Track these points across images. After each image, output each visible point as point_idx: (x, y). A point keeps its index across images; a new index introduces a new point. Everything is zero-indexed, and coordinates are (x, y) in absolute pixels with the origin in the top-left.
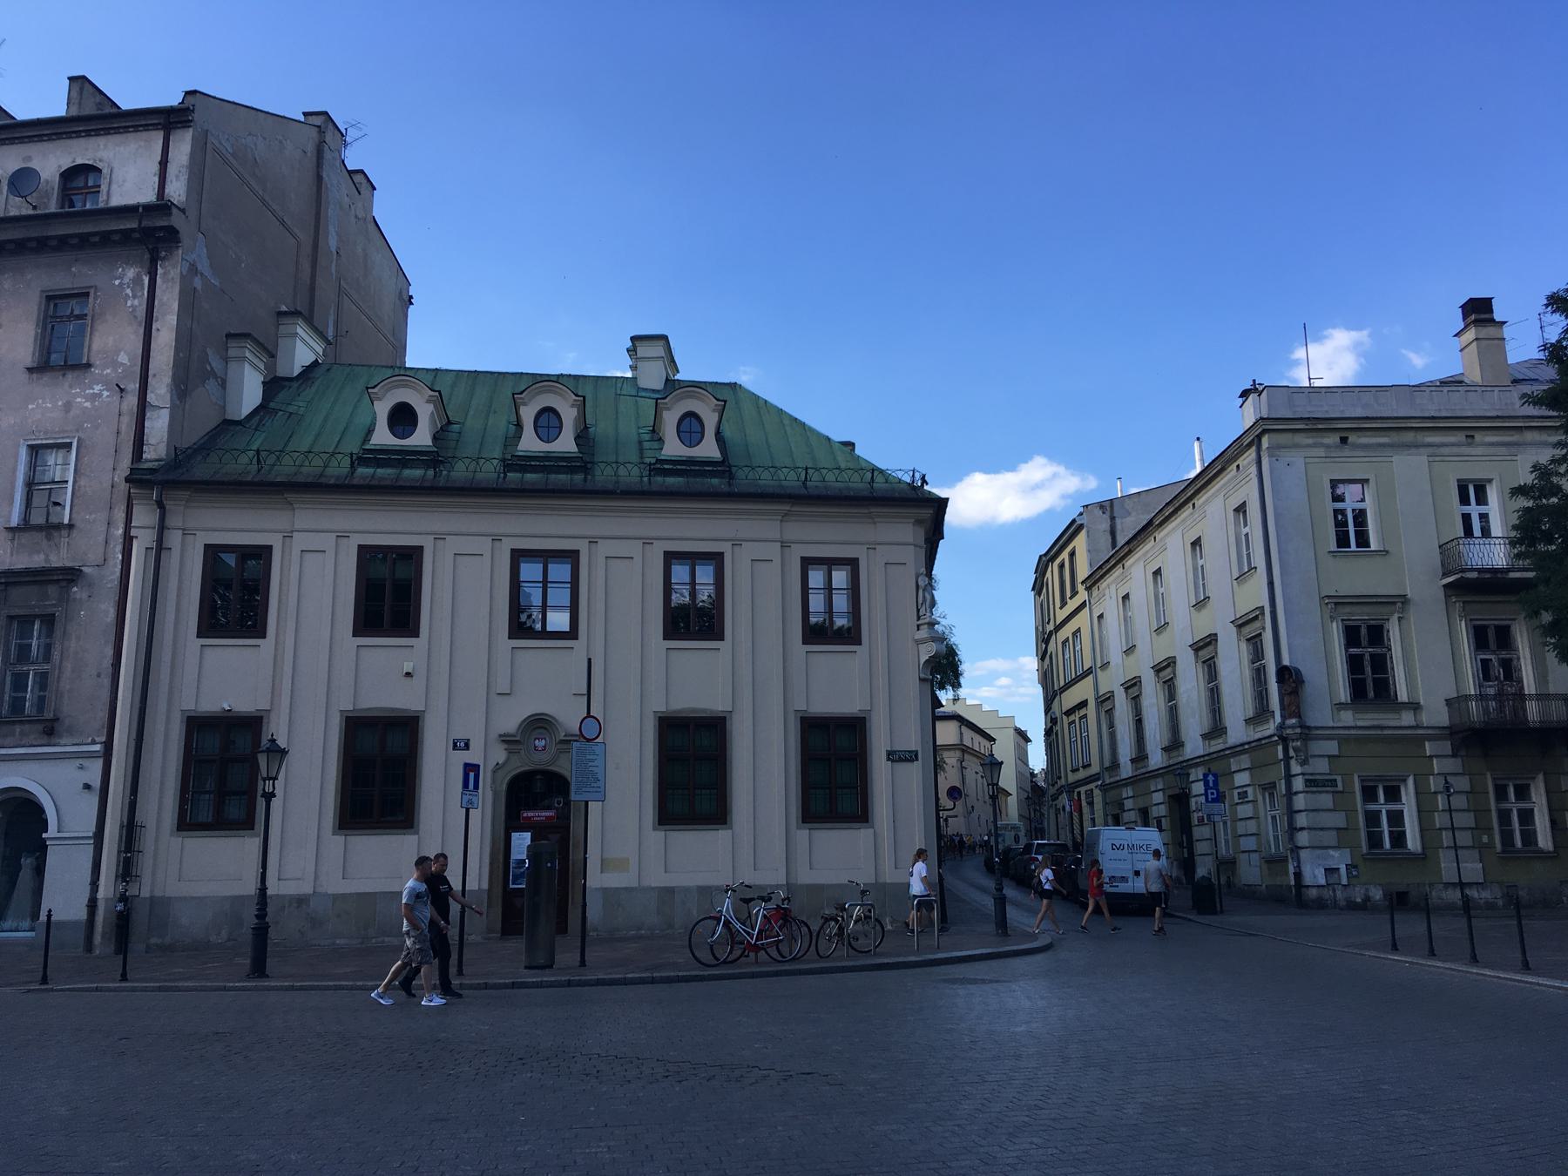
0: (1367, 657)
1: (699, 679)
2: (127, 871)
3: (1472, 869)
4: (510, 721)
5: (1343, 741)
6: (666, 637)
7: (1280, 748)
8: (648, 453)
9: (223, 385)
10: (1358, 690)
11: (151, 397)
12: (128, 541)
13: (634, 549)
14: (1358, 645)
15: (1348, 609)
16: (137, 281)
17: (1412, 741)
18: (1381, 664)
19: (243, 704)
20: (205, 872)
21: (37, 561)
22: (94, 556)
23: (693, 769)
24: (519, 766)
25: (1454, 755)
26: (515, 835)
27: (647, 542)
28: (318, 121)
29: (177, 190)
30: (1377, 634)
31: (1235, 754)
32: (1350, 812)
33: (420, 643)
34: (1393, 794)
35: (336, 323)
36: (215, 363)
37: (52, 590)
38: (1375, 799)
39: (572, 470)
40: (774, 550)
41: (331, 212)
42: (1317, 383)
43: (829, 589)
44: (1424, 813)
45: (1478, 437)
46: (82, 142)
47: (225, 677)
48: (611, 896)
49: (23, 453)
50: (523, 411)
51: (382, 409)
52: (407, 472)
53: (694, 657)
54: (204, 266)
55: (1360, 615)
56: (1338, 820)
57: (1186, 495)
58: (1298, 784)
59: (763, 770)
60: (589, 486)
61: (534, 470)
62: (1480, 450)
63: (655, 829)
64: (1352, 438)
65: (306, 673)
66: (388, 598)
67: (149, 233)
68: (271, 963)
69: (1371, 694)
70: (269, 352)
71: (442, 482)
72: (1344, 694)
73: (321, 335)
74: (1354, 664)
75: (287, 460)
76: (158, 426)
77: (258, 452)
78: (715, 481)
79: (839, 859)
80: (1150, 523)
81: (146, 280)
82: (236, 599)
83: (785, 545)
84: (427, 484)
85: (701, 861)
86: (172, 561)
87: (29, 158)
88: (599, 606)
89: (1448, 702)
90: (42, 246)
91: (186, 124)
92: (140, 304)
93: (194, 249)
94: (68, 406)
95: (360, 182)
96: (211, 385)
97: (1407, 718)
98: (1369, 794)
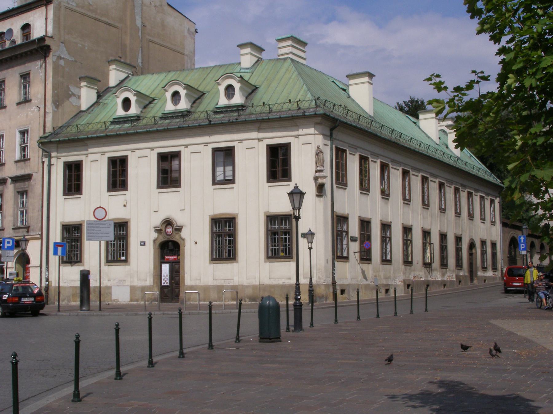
4: (157, 221)
11: (47, 110)
13: (200, 148)
16: (41, 66)
22: (36, 170)
23: (224, 236)
24: (162, 239)
26: (163, 265)
36: (73, 90)
48: (192, 287)
49: (18, 137)
59: (251, 238)
66: (168, 174)
67: (39, 49)
71: (242, 118)
81: (44, 65)
82: (74, 183)
87: (12, 24)
92: (42, 74)
94: (27, 115)
96: (73, 99)
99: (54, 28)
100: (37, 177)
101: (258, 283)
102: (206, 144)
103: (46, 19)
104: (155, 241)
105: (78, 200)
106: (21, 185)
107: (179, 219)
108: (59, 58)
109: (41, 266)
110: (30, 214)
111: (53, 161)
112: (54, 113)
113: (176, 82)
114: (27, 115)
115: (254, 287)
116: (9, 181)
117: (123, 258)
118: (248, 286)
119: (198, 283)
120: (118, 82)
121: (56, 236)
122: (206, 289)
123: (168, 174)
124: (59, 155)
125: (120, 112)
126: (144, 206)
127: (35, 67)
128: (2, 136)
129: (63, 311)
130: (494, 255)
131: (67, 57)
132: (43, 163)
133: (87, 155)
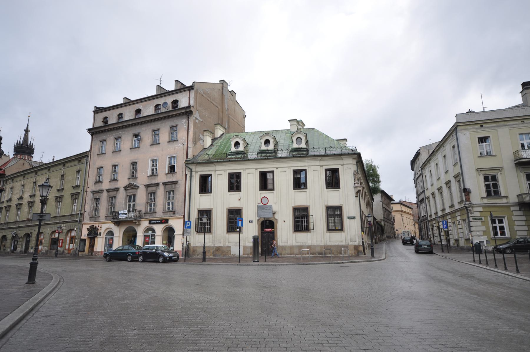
0: (491, 185)
1: (301, 198)
3: (484, 239)
5: (484, 207)
9: (203, 141)
10: (489, 194)
11: (189, 146)
12: (186, 175)
13: (222, 172)
14: (488, 181)
15: (484, 172)
16: (186, 122)
17: (507, 206)
18: (496, 186)
21: (170, 180)
22: (180, 178)
25: (520, 210)
27: (321, 166)
28: (222, 82)
29: (192, 103)
30: (494, 178)
31: (457, 212)
32: (487, 226)
34: (501, 221)
35: (228, 124)
36: (201, 136)
37: (173, 185)
38: (495, 223)
41: (226, 101)
42: (486, 110)
44: (511, 227)
45: (525, 121)
46: (158, 99)
47: (202, 202)
48: (283, 248)
49: (167, 159)
51: (233, 143)
53: (235, 195)
54: (198, 117)
55: (488, 173)
56: (484, 228)
57: (441, 145)
58: (471, 219)
61: (264, 153)
62: (526, 125)
64: (484, 125)
65: (220, 200)
66: (235, 183)
67: (187, 112)
69: (493, 194)
70: (213, 133)
72: (484, 194)
73: (224, 127)
74: (488, 186)
76: (190, 151)
79: (336, 239)
80: (434, 151)
82: (205, 185)
86: (193, 179)
89: (518, 196)
90: (169, 117)
91: (193, 89)
92: (186, 127)
93: (196, 115)
94: (175, 149)
95: (233, 93)
96: (201, 141)
97: (505, 201)
98: (493, 221)
99: (194, 102)
100: (181, 183)
101: (323, 244)
102: (289, 168)
103: (189, 98)
104: (258, 220)
105: (209, 197)
106: (169, 187)
108: (196, 118)
110: (176, 204)
111: (193, 174)
112: (193, 147)
113: (237, 137)
114: (175, 149)
115: (321, 247)
116: (161, 184)
117: (238, 230)
118: (317, 246)
119: (286, 244)
121: (194, 215)
122: (291, 247)
123: (235, 183)
127: (182, 123)
131: (199, 118)
132: (186, 175)
133: (215, 171)
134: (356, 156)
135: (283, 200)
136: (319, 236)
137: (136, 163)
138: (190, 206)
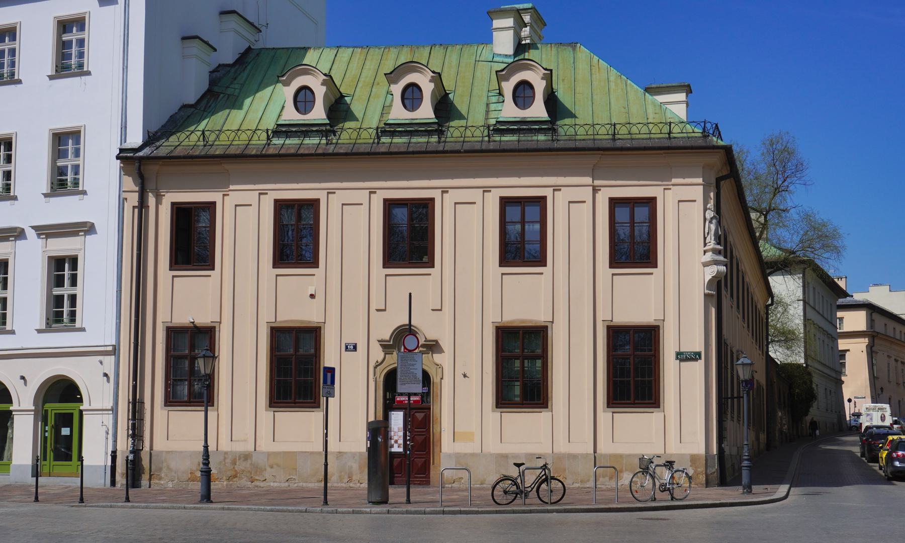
1: (525, 297)
2: (136, 433)
6: (275, 265)
7: (187, 363)
8: (493, 115)
19: (203, 320)
20: (176, 434)
33: (319, 272)
39: (429, 133)
40: (252, 197)
43: (632, 222)
48: (463, 463)
50: (504, 84)
52: (307, 141)
53: (407, 281)
59: (577, 367)
60: (556, 145)
61: (401, 134)
63: (493, 411)
66: (409, 239)
68: (39, 498)
71: (331, 149)
75: (223, 137)
77: (203, 132)
78: (541, 137)
82: (193, 244)
83: (595, 190)
84: (320, 151)
85: (526, 435)
88: (228, 242)
107: (428, 327)
109: (115, 410)
120: (237, 56)
123: (409, 239)
124: (597, 183)
125: (291, 115)
126: (351, 297)
128: (8, 144)
129: (46, 501)
130: (732, 412)
134: (716, 160)
135: (465, 296)
136: (576, 423)
137: (75, 135)
138: (125, 68)
